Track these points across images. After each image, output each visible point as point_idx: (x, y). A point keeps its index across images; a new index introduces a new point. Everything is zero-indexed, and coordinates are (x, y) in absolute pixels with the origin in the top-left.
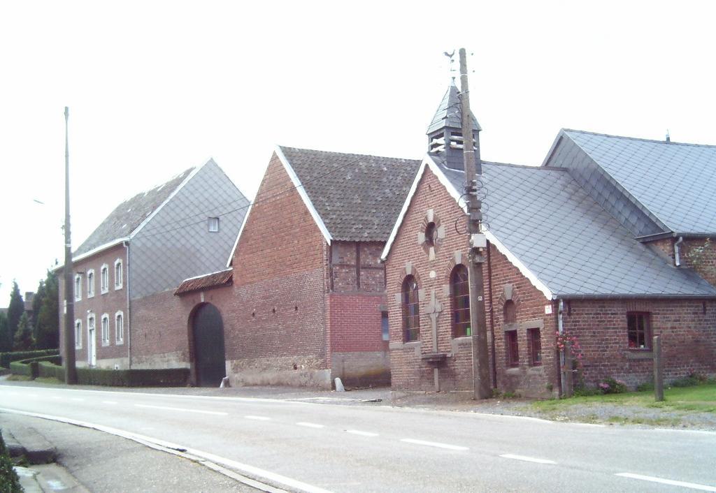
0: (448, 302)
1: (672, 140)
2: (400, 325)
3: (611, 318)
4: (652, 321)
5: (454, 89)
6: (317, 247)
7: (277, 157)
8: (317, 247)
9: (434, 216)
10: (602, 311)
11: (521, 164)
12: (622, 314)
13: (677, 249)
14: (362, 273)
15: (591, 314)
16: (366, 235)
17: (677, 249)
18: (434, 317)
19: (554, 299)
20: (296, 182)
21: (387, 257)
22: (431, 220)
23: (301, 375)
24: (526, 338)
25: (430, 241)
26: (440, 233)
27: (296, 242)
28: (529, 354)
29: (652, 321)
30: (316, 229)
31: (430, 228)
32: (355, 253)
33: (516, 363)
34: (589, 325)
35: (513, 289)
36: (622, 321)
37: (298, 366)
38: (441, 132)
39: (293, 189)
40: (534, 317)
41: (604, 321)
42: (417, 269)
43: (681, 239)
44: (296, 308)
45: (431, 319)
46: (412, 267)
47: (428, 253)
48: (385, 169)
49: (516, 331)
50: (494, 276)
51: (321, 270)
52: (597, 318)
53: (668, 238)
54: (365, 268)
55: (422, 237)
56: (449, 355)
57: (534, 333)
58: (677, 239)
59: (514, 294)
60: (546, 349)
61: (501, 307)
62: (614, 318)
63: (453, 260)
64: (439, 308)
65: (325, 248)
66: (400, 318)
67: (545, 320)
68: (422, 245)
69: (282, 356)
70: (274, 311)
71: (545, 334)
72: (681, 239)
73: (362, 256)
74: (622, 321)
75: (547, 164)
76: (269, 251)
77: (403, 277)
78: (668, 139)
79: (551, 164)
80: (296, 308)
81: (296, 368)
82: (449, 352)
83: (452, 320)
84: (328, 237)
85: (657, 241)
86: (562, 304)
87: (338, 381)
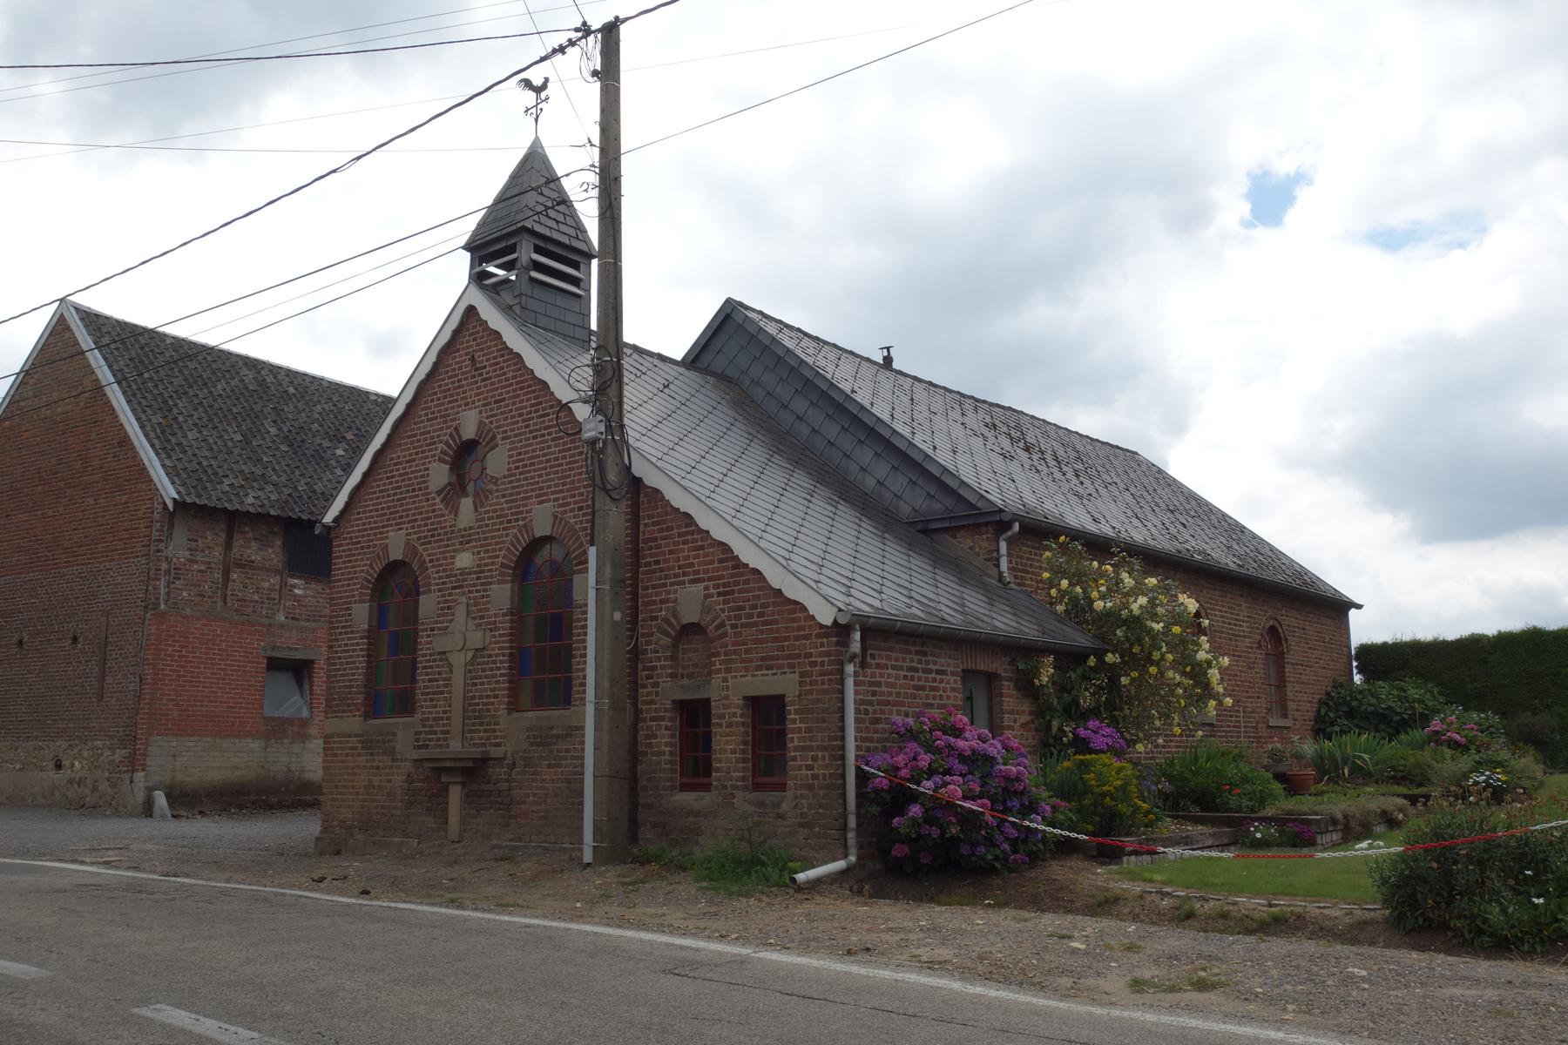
0: (505, 625)
1: (895, 365)
2: (359, 678)
3: (934, 680)
4: (1001, 695)
5: (534, 176)
6: (140, 514)
7: (68, 329)
8: (140, 514)
9: (481, 424)
10: (920, 662)
11: (656, 351)
12: (953, 674)
13: (1003, 546)
14: (235, 576)
15: (901, 668)
16: (250, 500)
17: (1003, 546)
18: (459, 661)
19: (840, 621)
20: (105, 375)
21: (336, 520)
22: (469, 432)
23: (71, 782)
24: (739, 711)
25: (457, 487)
26: (497, 462)
27: (91, 501)
28: (744, 760)
29: (1001, 695)
30: (142, 473)
31: (465, 453)
32: (223, 535)
33: (705, 780)
34: (898, 694)
35: (706, 596)
36: (953, 690)
37: (66, 763)
38: (511, 242)
39: (98, 389)
40: (769, 668)
41: (922, 688)
42: (420, 548)
43: (1016, 527)
44: (75, 639)
45: (451, 665)
46: (407, 543)
47: (455, 511)
48: (291, 390)
49: (708, 701)
50: (648, 564)
51: (143, 560)
52: (912, 678)
53: (987, 524)
54: (243, 566)
55: (439, 474)
56: (496, 752)
57: (766, 713)
58: (1008, 526)
59: (706, 610)
60: (804, 748)
61: (666, 640)
62: (941, 681)
63: (527, 528)
64: (476, 639)
65: (156, 516)
66: (361, 663)
67: (802, 675)
68: (439, 493)
69: (28, 739)
70: (20, 643)
71: (796, 711)
72: (1016, 527)
73: (238, 543)
74: (953, 690)
75: (693, 361)
76: (24, 517)
77: (378, 567)
78: (888, 360)
79: (704, 362)
80: (75, 639)
81: (58, 766)
82: (499, 745)
83: (511, 668)
84: (169, 491)
85: (977, 526)
86: (857, 636)
87: (160, 799)
